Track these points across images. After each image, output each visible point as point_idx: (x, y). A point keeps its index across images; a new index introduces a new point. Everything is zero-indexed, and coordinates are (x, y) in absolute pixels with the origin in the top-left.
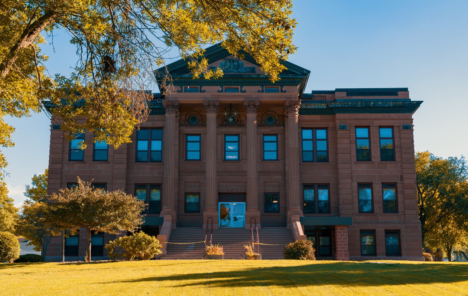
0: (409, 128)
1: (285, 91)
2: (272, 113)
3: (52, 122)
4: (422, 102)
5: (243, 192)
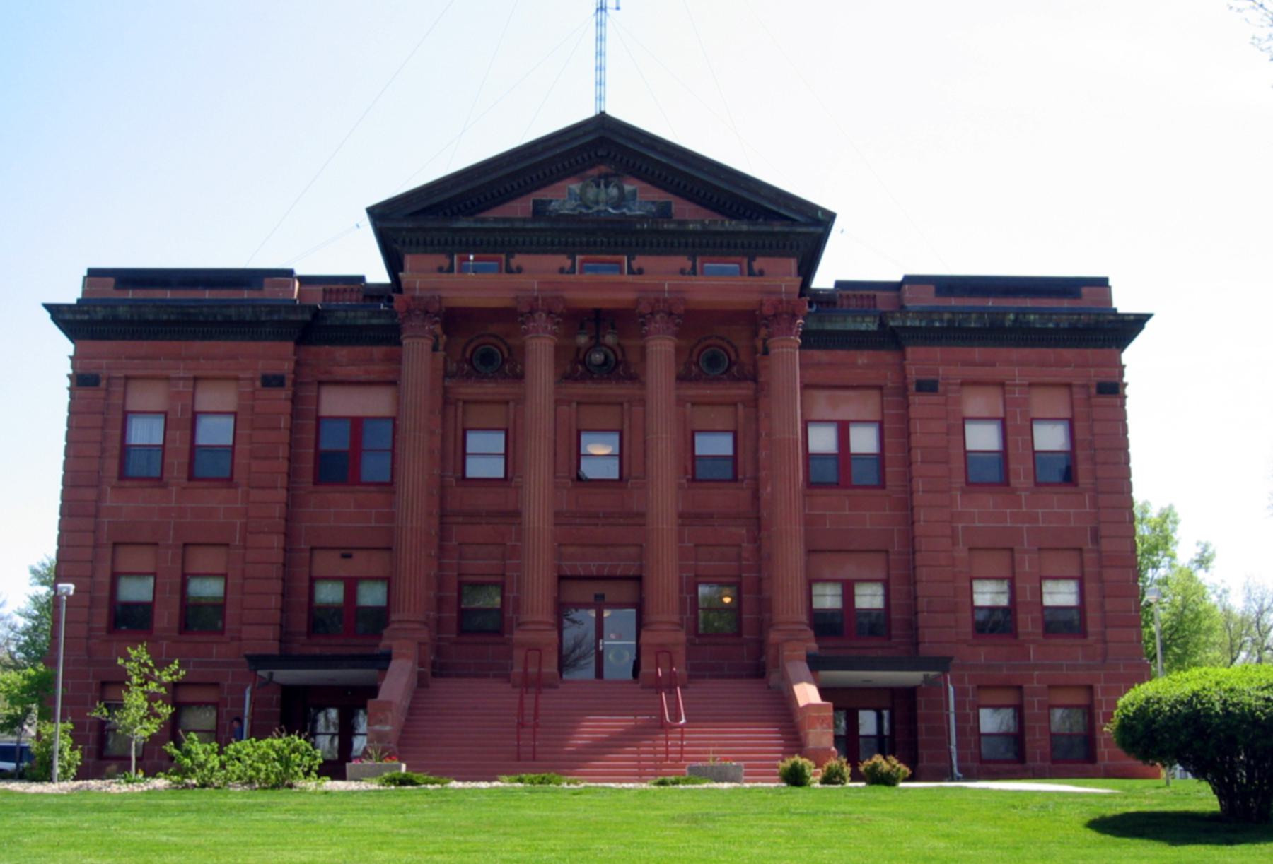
0: (1114, 389)
1: (761, 273)
2: (720, 342)
3: (73, 367)
4: (1147, 317)
5: (631, 573)
